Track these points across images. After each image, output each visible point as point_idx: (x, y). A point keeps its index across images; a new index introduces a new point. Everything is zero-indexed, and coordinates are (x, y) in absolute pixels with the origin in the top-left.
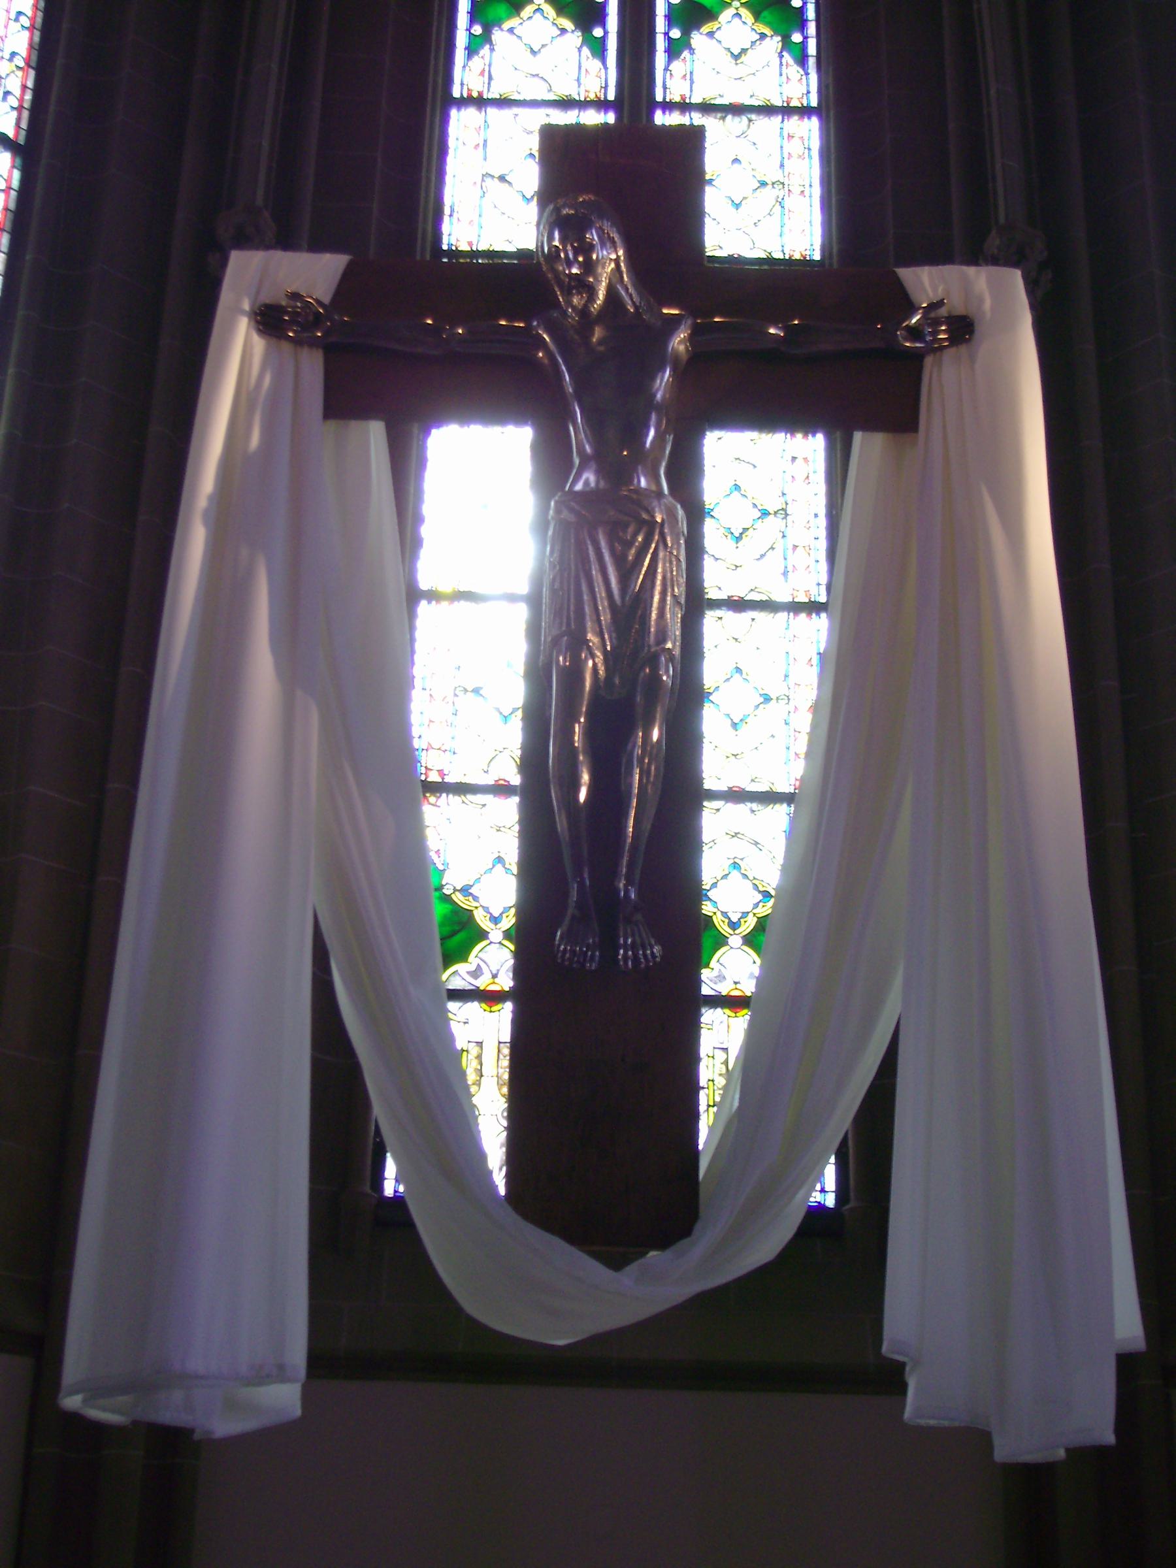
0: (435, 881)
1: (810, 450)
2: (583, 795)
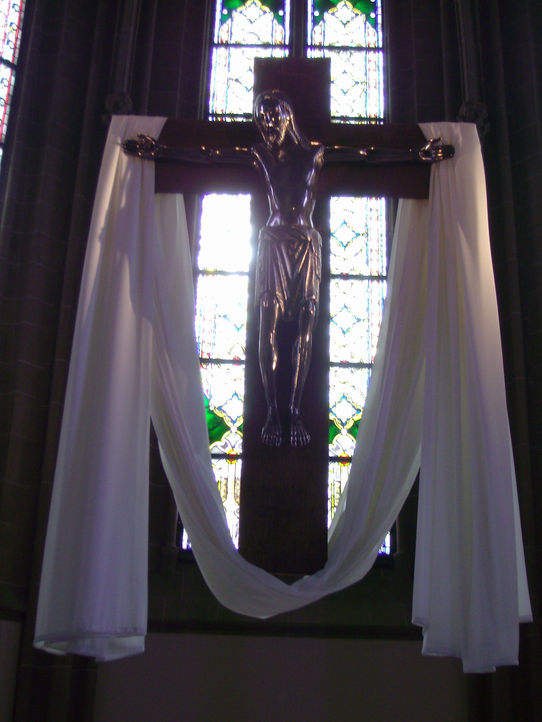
0: (206, 404)
1: (378, 205)
2: (274, 366)
